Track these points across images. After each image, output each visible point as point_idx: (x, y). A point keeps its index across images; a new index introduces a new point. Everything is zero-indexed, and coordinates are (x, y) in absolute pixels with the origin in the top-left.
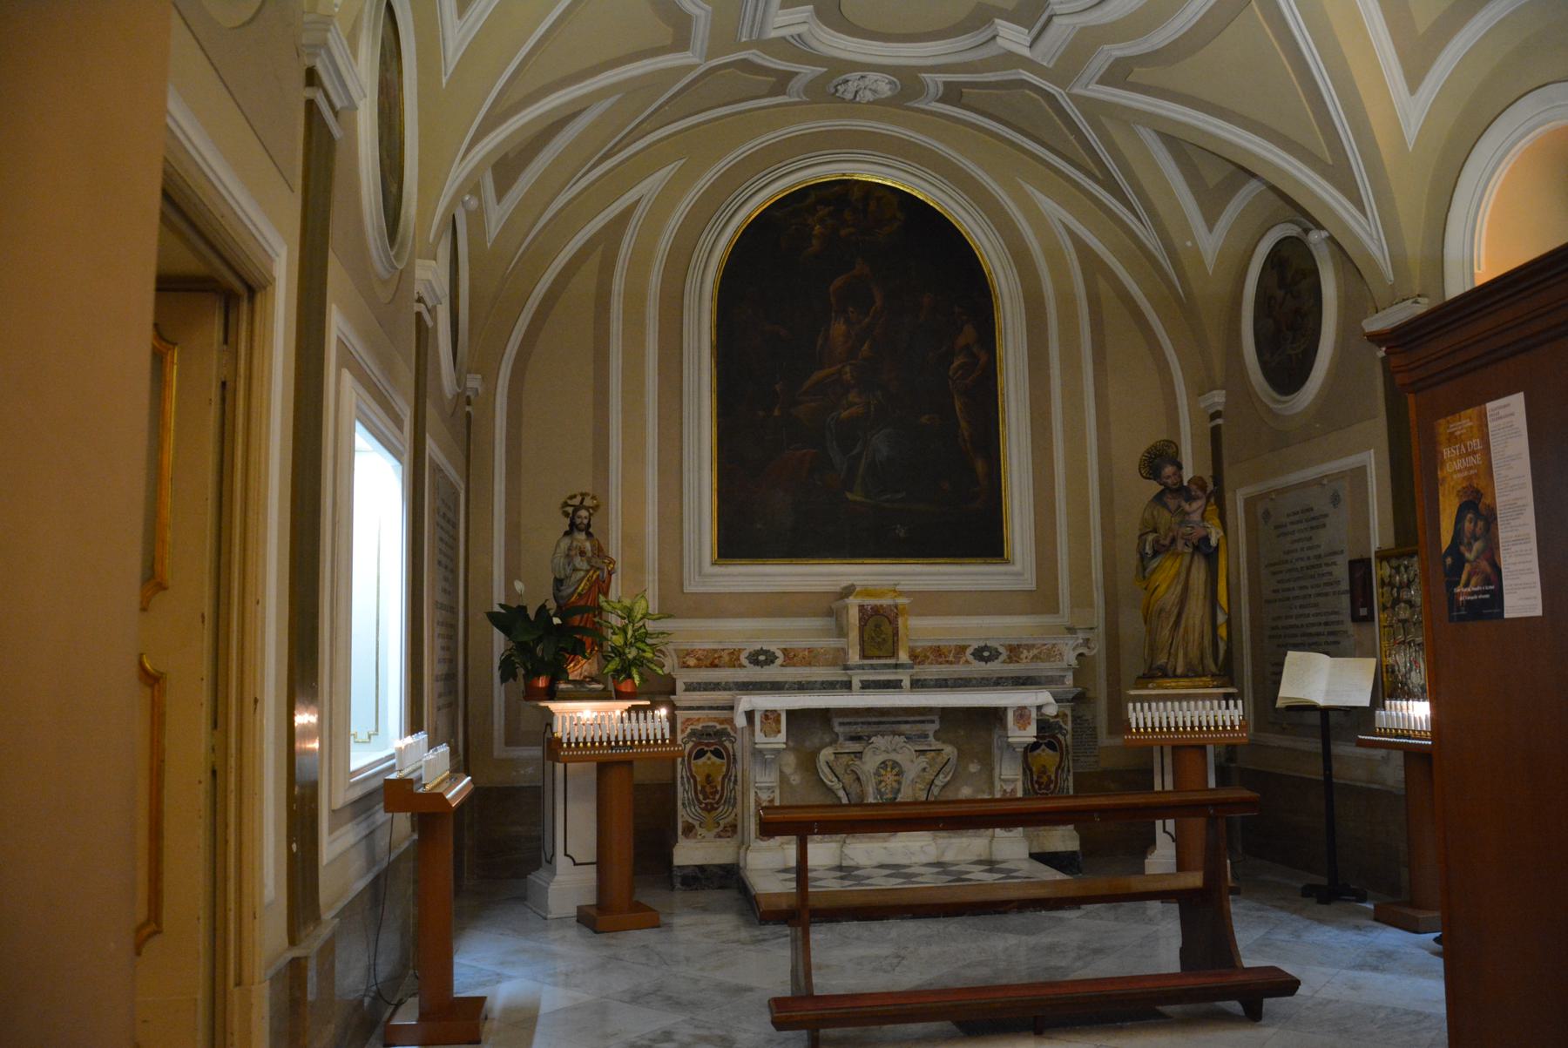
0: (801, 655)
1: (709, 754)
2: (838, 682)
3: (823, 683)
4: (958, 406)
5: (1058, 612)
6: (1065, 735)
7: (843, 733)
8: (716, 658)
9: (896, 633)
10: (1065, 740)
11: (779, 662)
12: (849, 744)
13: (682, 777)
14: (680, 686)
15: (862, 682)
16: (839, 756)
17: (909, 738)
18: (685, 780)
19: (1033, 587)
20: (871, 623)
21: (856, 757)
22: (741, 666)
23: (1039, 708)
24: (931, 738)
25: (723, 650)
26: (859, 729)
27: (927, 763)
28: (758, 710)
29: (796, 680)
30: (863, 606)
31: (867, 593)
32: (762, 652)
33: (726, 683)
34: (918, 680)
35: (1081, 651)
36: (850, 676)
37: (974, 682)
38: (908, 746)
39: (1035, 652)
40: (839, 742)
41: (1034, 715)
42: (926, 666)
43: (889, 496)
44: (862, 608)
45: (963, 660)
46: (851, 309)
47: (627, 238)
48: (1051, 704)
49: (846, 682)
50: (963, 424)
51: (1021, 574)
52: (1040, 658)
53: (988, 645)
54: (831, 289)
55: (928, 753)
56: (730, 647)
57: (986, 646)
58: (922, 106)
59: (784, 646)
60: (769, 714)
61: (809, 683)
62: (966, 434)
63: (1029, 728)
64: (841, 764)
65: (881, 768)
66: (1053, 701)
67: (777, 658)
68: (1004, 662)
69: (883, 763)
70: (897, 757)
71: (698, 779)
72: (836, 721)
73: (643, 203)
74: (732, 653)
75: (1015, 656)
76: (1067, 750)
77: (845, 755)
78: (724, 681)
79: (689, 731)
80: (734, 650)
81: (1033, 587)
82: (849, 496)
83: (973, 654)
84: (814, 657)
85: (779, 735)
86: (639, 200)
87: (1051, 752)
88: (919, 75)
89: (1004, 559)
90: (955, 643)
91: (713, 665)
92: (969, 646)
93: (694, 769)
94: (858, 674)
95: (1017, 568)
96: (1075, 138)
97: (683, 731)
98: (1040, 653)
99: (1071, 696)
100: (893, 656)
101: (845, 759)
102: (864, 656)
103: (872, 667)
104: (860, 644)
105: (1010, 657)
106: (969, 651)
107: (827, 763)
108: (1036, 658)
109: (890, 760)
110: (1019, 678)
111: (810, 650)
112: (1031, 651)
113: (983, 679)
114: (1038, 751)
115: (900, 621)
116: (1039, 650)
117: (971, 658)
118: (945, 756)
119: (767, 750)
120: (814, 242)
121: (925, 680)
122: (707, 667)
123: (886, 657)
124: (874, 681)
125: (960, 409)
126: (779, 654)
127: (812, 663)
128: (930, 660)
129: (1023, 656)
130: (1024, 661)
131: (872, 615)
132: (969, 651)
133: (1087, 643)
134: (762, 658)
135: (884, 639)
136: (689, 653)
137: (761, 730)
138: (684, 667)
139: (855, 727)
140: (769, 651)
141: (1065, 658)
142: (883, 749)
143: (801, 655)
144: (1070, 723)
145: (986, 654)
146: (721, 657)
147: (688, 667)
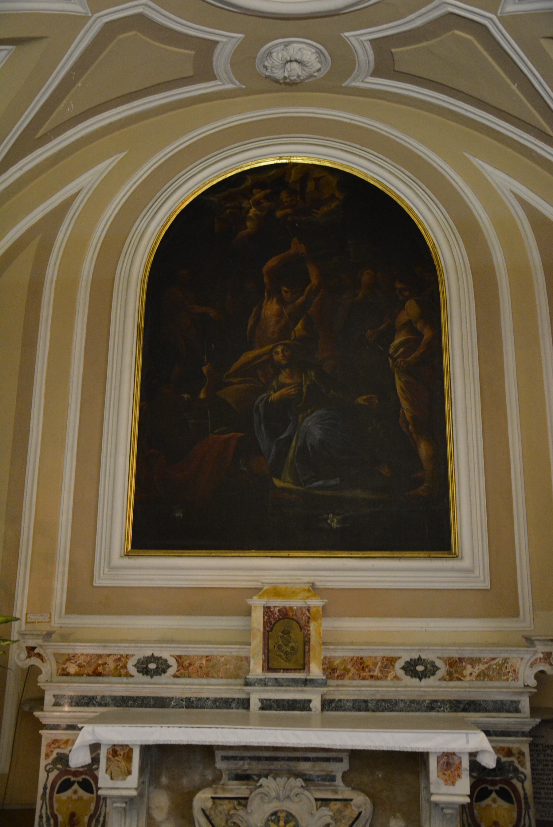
0: (197, 665)
1: (76, 786)
2: (234, 699)
3: (216, 700)
4: (399, 384)
5: (517, 615)
6: (522, 781)
7: (227, 770)
8: (99, 665)
9: (307, 642)
10: (524, 789)
11: (172, 671)
12: (234, 785)
13: (41, 817)
14: (49, 699)
15: (262, 701)
16: (218, 802)
17: (308, 780)
18: (44, 819)
19: (487, 585)
20: (278, 628)
21: (240, 804)
22: (128, 675)
23: (473, 755)
24: (339, 781)
25: (109, 655)
26: (246, 767)
27: (332, 817)
28: (104, 745)
29: (184, 696)
30: (269, 608)
31: (276, 592)
32: (153, 659)
33: (103, 697)
34: (332, 701)
35: (541, 668)
36: (249, 694)
37: (402, 705)
38: (306, 793)
39: (482, 667)
40: (222, 782)
41: (466, 764)
42: (346, 682)
43: (320, 483)
44: (267, 610)
45: (391, 675)
46: (285, 289)
47: (63, 229)
48: (489, 752)
49: (243, 699)
50: (404, 404)
51: (472, 571)
52: (488, 676)
53: (423, 657)
54: (265, 269)
55: (333, 803)
56: (116, 652)
57: (419, 658)
58: (358, 84)
59: (178, 653)
60: (118, 749)
61: (199, 699)
62: (408, 415)
63: (459, 782)
64: (221, 813)
65: (272, 821)
66: (491, 750)
67: (169, 666)
68: (443, 679)
69: (275, 814)
70: (293, 807)
71: (60, 819)
72: (219, 754)
73: (80, 197)
74: (119, 659)
75: (456, 672)
76: (527, 803)
77: (226, 801)
78: (99, 694)
79: (54, 755)
80: (122, 656)
81: (487, 585)
82: (278, 483)
83: (403, 668)
84: (213, 666)
85: (129, 778)
86: (79, 192)
87: (505, 805)
88: (342, 35)
89: (451, 554)
90: (381, 654)
91: (97, 674)
92: (399, 658)
93: (56, 806)
94: (257, 691)
95: (466, 563)
96: (518, 87)
97: (47, 756)
98: (488, 668)
99: (527, 729)
100: (304, 669)
101: (226, 806)
102: (268, 667)
103: (278, 683)
104: (264, 653)
105: (450, 674)
106: (400, 664)
107: (203, 810)
108: (483, 675)
109: (282, 811)
110: (458, 702)
111: (208, 658)
112: (477, 667)
113: (412, 702)
114: (488, 801)
115: (313, 626)
116: (486, 666)
117: (401, 673)
118: (354, 808)
119: (112, 797)
120: (248, 224)
121: (340, 700)
122: (89, 675)
123: (295, 670)
124: (277, 701)
125: (401, 388)
126: (172, 662)
127: (210, 675)
128: (350, 674)
129: (467, 672)
130: (468, 678)
131: (280, 619)
132: (400, 664)
133: (549, 658)
134: (152, 666)
135: (293, 648)
136: (70, 658)
137: (107, 770)
138: (63, 675)
139: (241, 763)
140: (161, 657)
141: (519, 676)
142: (273, 794)
143: (197, 665)
144: (528, 764)
145: (420, 668)
146: (106, 663)
147: (68, 674)
